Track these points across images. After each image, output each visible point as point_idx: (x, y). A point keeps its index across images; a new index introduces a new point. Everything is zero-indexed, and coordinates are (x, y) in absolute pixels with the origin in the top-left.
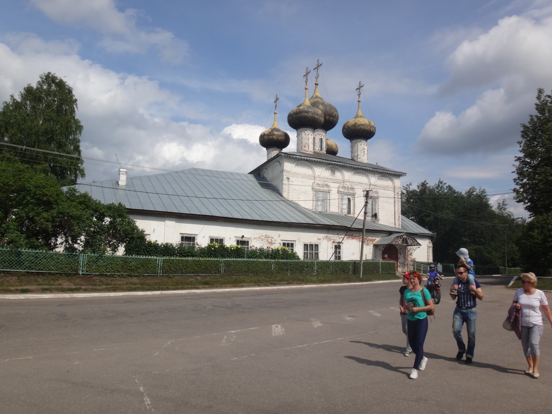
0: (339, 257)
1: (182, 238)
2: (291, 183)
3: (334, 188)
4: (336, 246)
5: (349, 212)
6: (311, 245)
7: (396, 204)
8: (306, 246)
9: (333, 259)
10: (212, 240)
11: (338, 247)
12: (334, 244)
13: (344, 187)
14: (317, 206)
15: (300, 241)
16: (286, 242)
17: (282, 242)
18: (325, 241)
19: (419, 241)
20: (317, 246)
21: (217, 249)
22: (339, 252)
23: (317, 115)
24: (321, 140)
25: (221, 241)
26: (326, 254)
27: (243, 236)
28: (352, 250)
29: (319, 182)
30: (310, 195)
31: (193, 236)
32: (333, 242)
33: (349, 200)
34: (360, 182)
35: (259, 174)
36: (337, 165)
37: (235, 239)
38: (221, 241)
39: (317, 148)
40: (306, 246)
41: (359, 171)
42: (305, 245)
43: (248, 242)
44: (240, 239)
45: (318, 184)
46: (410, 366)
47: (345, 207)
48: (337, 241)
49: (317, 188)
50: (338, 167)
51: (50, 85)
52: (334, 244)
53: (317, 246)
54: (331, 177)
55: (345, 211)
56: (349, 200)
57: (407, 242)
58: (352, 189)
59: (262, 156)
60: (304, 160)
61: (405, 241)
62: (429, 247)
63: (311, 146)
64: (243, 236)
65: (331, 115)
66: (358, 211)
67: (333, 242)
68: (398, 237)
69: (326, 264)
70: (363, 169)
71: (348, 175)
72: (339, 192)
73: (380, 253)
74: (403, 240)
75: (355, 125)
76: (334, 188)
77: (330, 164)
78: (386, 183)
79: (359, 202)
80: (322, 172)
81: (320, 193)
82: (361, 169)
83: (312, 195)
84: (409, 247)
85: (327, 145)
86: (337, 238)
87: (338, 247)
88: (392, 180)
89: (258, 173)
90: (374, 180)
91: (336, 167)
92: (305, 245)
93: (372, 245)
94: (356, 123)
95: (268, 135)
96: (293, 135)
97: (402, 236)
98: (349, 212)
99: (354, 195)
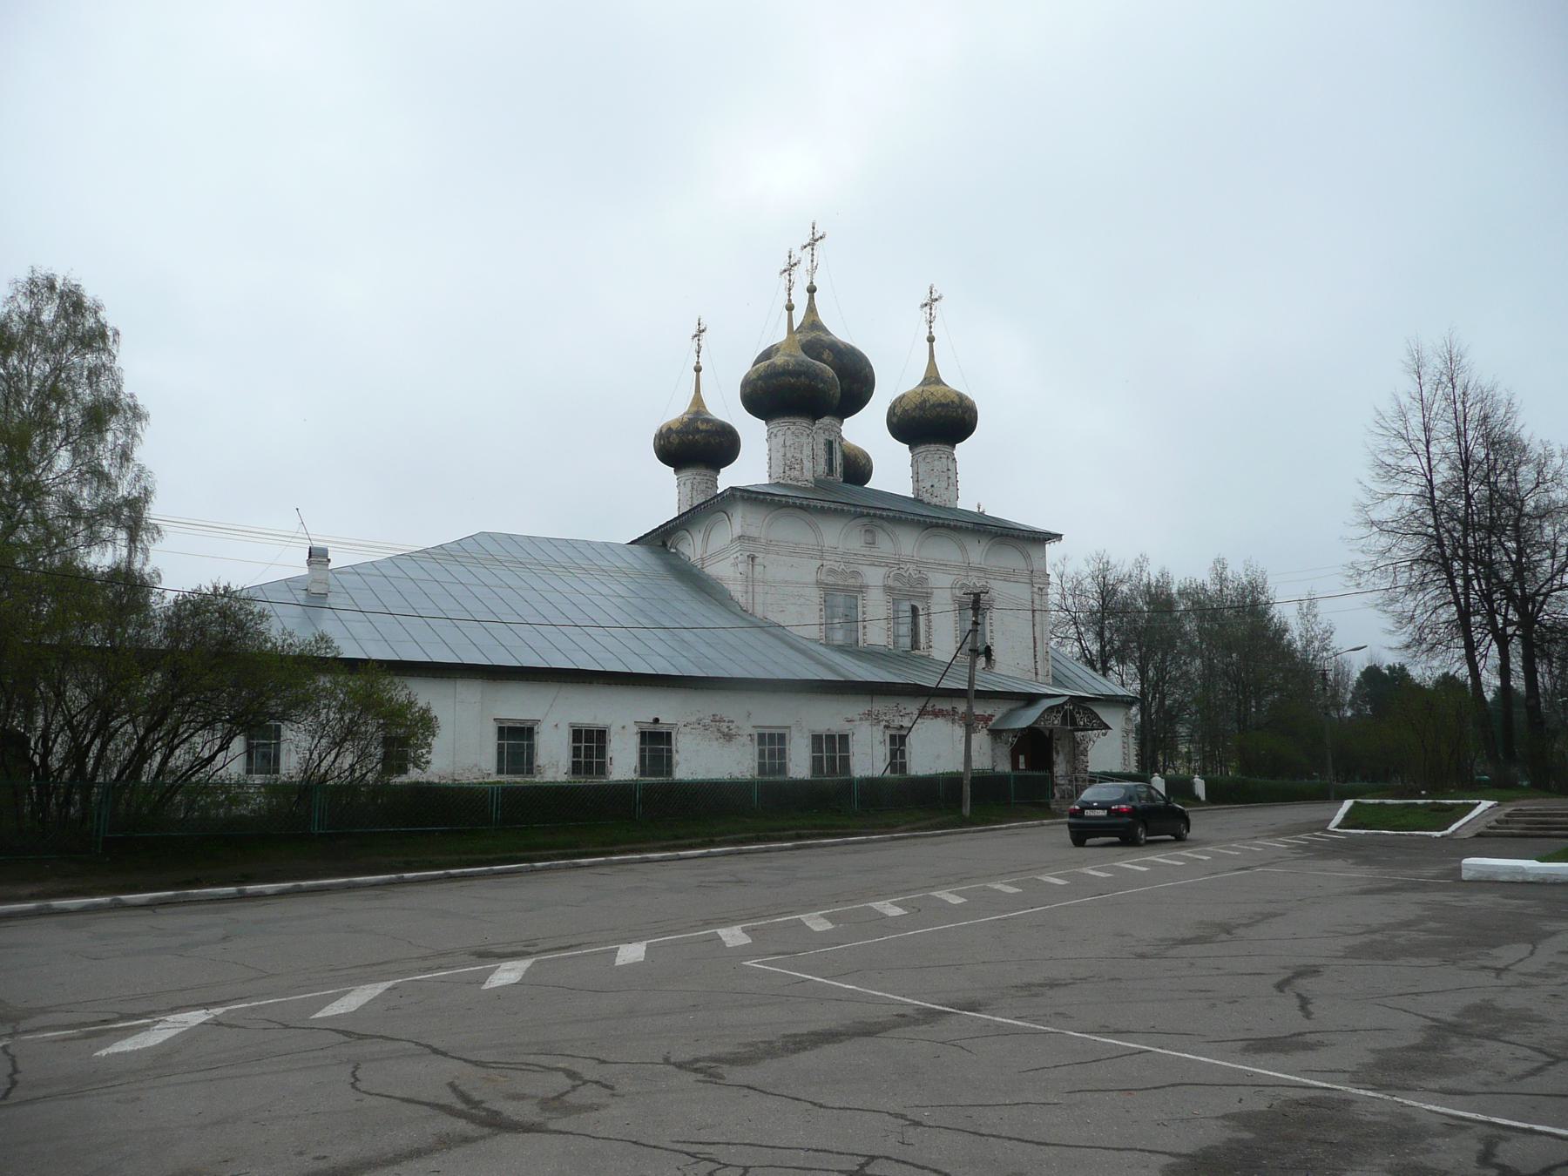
0: (903, 766)
1: (501, 730)
2: (758, 569)
3: (874, 577)
4: (893, 738)
5: (915, 644)
6: (831, 738)
8: (817, 739)
11: (898, 743)
12: (889, 733)
14: (897, 636)
16: (767, 731)
17: (755, 732)
18: (866, 724)
19: (1106, 715)
20: (844, 738)
22: (903, 753)
23: (824, 382)
26: (868, 759)
27: (656, 721)
28: (937, 749)
29: (836, 566)
30: (815, 595)
31: (529, 724)
32: (887, 727)
33: (914, 610)
35: (664, 544)
36: (881, 517)
37: (636, 729)
39: (822, 468)
40: (817, 739)
41: (935, 531)
42: (814, 737)
43: (669, 734)
44: (652, 728)
45: (832, 572)
46: (759, 1170)
47: (905, 629)
48: (896, 723)
49: (831, 580)
50: (885, 524)
52: (889, 733)
53: (844, 738)
55: (906, 642)
56: (914, 610)
57: (1074, 722)
58: (856, 574)
59: (662, 494)
60: (794, 506)
61: (1070, 719)
62: (1127, 732)
63: (808, 464)
64: (656, 721)
66: (943, 639)
67: (887, 727)
68: (1051, 708)
69: (870, 784)
70: (948, 527)
71: (907, 544)
72: (888, 589)
73: (1005, 750)
74: (1064, 716)
76: (874, 577)
77: (862, 515)
79: (876, 606)
80: (839, 538)
81: (841, 597)
82: (943, 526)
83: (818, 600)
84: (1079, 734)
85: (845, 457)
87: (898, 743)
88: (963, 549)
89: (661, 540)
90: (977, 552)
91: (878, 522)
92: (814, 737)
93: (985, 731)
94: (925, 401)
95: (678, 432)
96: (753, 432)
97: (1062, 705)
99: (927, 596)
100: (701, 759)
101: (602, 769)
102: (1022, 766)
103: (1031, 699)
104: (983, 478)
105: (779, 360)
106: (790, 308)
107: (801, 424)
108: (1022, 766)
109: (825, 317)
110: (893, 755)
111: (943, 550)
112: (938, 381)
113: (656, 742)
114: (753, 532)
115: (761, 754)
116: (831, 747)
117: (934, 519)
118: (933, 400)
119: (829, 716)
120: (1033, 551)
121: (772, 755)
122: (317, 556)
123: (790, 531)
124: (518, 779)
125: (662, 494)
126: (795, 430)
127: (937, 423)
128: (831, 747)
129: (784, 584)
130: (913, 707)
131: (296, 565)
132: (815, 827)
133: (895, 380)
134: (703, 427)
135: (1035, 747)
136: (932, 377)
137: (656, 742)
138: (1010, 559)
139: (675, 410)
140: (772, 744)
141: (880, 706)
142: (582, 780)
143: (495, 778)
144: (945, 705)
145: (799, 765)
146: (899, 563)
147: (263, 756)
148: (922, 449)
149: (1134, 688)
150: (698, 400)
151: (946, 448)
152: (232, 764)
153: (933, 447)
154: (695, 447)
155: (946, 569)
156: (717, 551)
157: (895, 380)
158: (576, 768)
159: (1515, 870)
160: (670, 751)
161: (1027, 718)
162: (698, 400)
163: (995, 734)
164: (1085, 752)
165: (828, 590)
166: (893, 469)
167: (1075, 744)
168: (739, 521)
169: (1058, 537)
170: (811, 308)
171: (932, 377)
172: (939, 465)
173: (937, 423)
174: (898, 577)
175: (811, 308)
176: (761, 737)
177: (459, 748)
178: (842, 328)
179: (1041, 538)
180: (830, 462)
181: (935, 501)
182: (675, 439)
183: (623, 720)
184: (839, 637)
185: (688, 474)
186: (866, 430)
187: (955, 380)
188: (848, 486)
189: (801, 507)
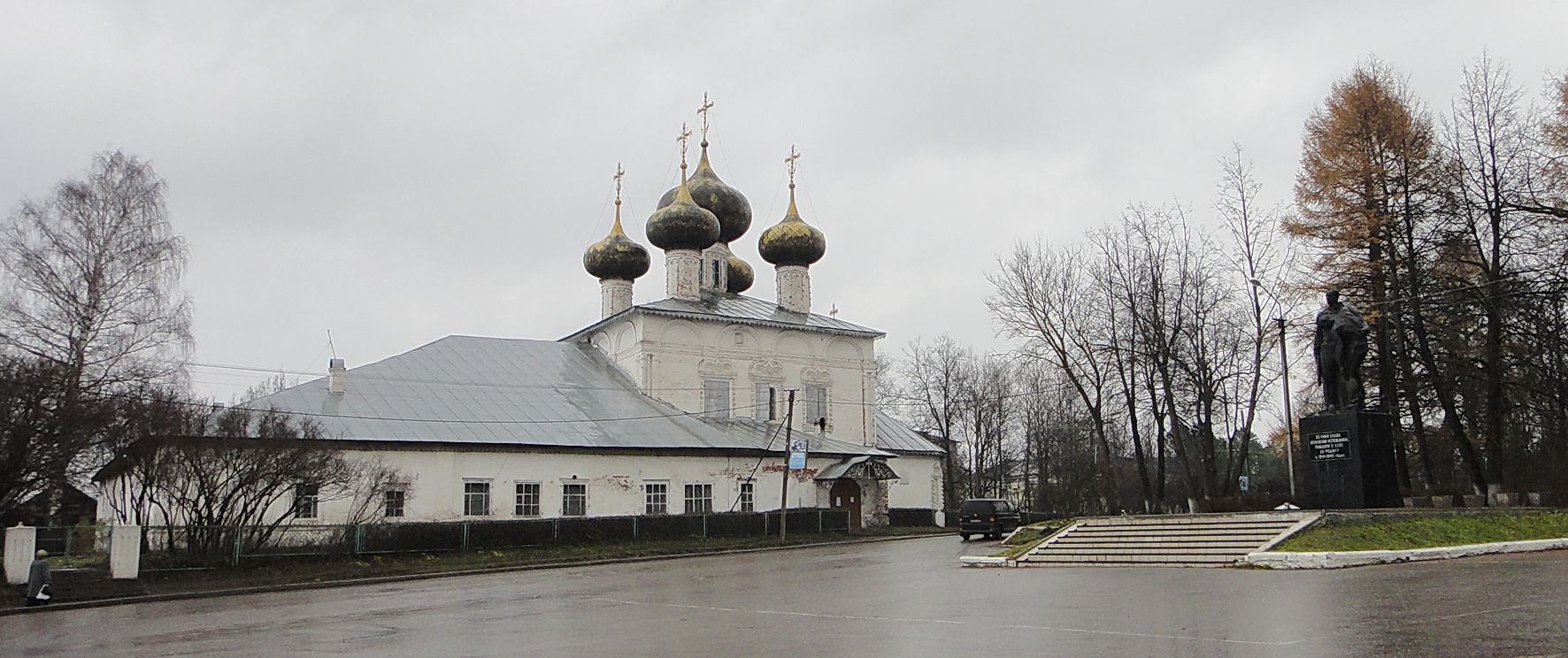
3: (742, 368)
9: (738, 508)
11: (747, 487)
20: (708, 487)
24: (716, 263)
26: (725, 501)
33: (772, 390)
53: (708, 487)
56: (772, 390)
57: (873, 474)
73: (825, 494)
76: (742, 368)
81: (716, 389)
85: (730, 267)
87: (747, 487)
89: (585, 340)
90: (820, 346)
96: (656, 254)
100: (600, 505)
101: (536, 511)
102: (838, 503)
103: (846, 457)
104: (829, 290)
105: (674, 208)
106: (684, 167)
107: (691, 254)
108: (838, 503)
109: (714, 167)
111: (795, 346)
112: (797, 218)
113: (574, 492)
115: (649, 499)
117: (789, 321)
120: (863, 344)
121: (656, 498)
123: (680, 334)
124: (478, 518)
125: (591, 299)
126: (685, 258)
127: (796, 251)
128: (697, 492)
129: (674, 379)
130: (752, 463)
132: (653, 553)
133: (765, 219)
134: (620, 249)
135: (845, 488)
136: (793, 217)
137: (574, 492)
138: (846, 350)
139: (598, 237)
140: (656, 491)
141: (736, 464)
142: (522, 518)
143: (463, 518)
145: (675, 505)
147: (304, 504)
148: (783, 269)
149: (759, 508)
150: (618, 227)
151: (802, 269)
152: (280, 505)
154: (618, 264)
155: (794, 362)
156: (624, 349)
157: (765, 219)
158: (519, 511)
160: (487, 497)
161: (840, 471)
162: (618, 227)
163: (818, 482)
164: (885, 495)
166: (766, 282)
167: (879, 488)
168: (638, 330)
169: (882, 335)
170: (704, 159)
171: (793, 217)
173: (796, 251)
175: (704, 159)
176: (649, 487)
177: (435, 496)
178: (730, 178)
179: (869, 336)
180: (716, 278)
181: (792, 308)
183: (551, 476)
185: (610, 283)
186: (745, 250)
187: (812, 219)
189: (691, 319)
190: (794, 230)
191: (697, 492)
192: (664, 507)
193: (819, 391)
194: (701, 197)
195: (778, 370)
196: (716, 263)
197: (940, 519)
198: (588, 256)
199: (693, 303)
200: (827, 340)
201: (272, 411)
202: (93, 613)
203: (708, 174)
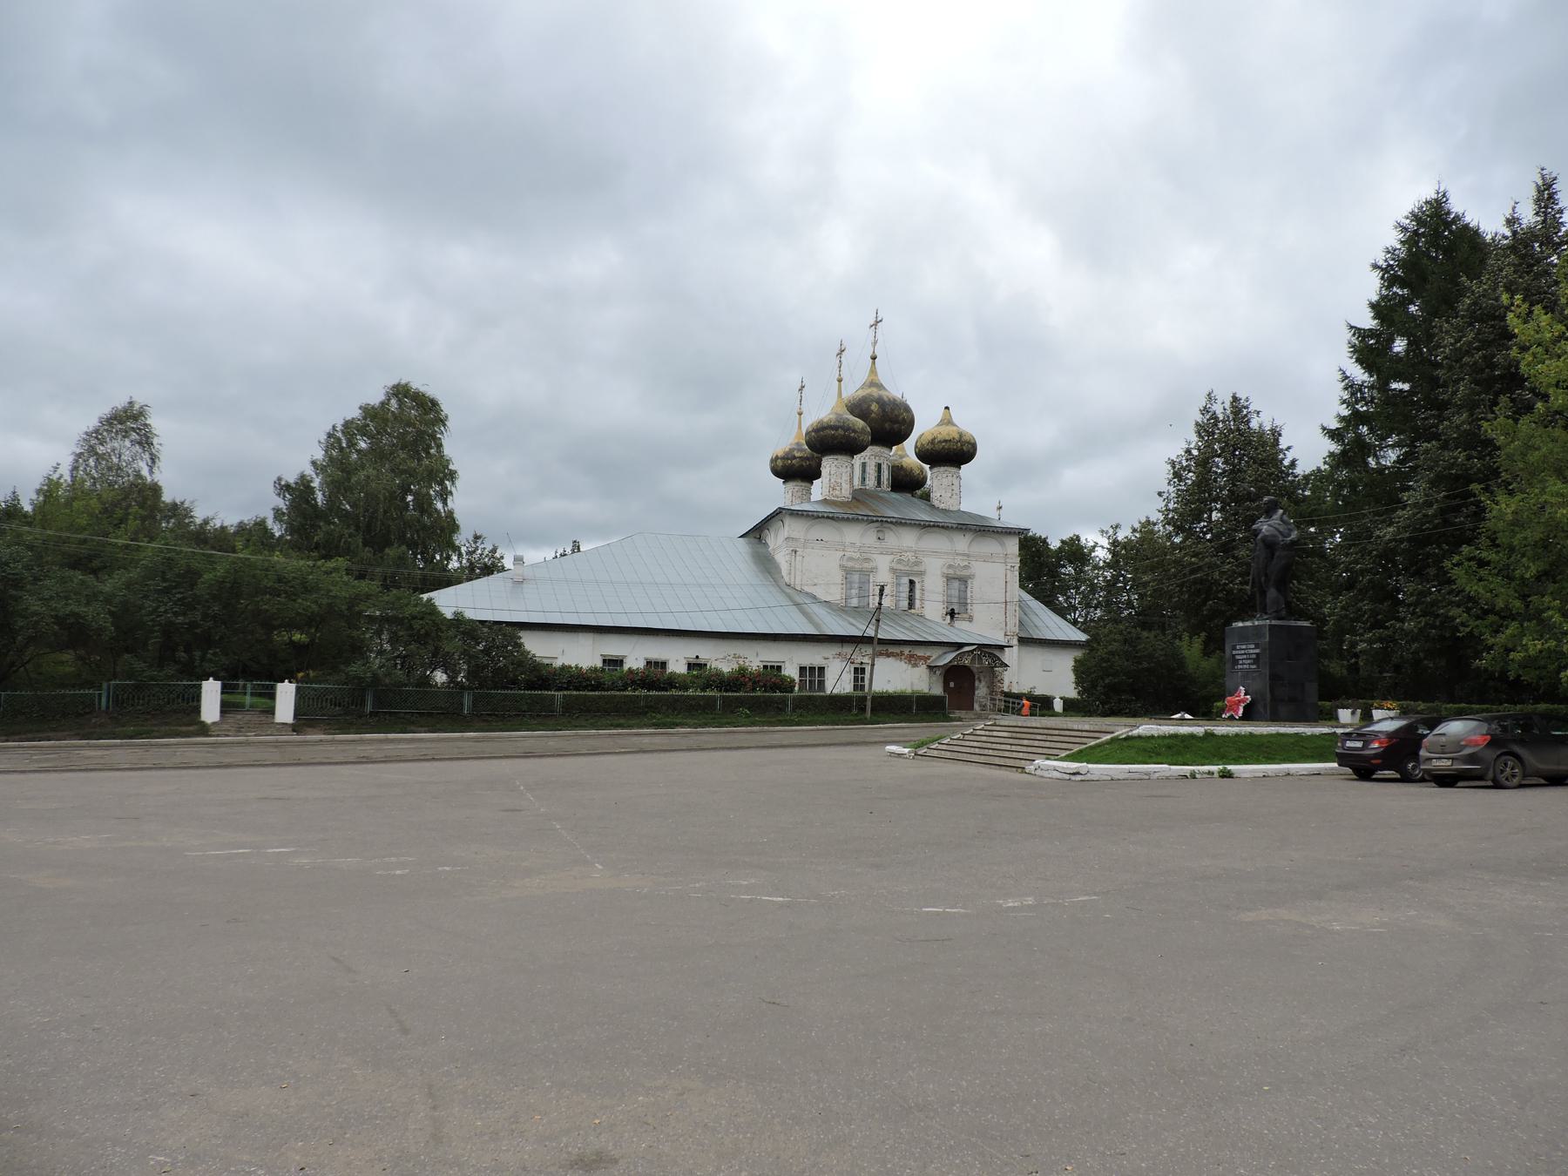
4: (856, 670)
5: (911, 605)
6: (812, 669)
7: (227, 760)
10: (649, 663)
11: (859, 671)
13: (900, 561)
15: (792, 662)
20: (822, 669)
21: (739, 680)
24: (879, 466)
25: (664, 664)
26: (838, 681)
28: (892, 677)
30: (838, 576)
33: (912, 582)
34: (936, 557)
38: (664, 664)
45: (850, 559)
47: (905, 595)
49: (850, 564)
51: (400, 402)
53: (822, 669)
54: (878, 544)
55: (905, 604)
56: (912, 582)
58: (867, 560)
65: (895, 420)
66: (932, 607)
72: (893, 570)
75: (932, 442)
78: (990, 546)
81: (856, 575)
86: (863, 656)
88: (1003, 544)
90: (962, 543)
95: (783, 458)
98: (911, 605)
99: (921, 574)
109: (883, 378)
110: (856, 679)
114: (795, 535)
116: (814, 674)
118: (940, 437)
119: (812, 656)
122: (1375, 266)
123: (826, 532)
127: (953, 453)
129: (825, 570)
131: (1376, 275)
133: (925, 425)
134: (797, 454)
136: (947, 421)
144: (892, 649)
146: (901, 552)
151: (953, 470)
153: (942, 469)
157: (925, 425)
159: (1122, 771)
163: (930, 668)
165: (848, 572)
170: (873, 371)
171: (947, 421)
172: (945, 482)
173: (953, 453)
174: (900, 561)
175: (873, 371)
181: (942, 506)
182: (780, 463)
184: (854, 602)
185: (791, 485)
188: (894, 495)
190: (947, 432)
191: (814, 674)
192: (822, 683)
193: (959, 580)
194: (858, 408)
195: (917, 563)
196: (879, 466)
197: (1058, 706)
198: (774, 460)
199: (843, 504)
200: (969, 537)
201: (1173, 464)
202: (891, 690)
203: (874, 384)
